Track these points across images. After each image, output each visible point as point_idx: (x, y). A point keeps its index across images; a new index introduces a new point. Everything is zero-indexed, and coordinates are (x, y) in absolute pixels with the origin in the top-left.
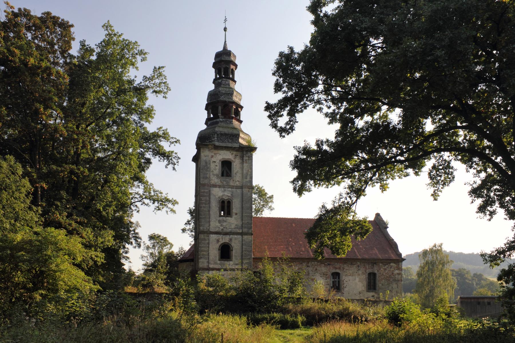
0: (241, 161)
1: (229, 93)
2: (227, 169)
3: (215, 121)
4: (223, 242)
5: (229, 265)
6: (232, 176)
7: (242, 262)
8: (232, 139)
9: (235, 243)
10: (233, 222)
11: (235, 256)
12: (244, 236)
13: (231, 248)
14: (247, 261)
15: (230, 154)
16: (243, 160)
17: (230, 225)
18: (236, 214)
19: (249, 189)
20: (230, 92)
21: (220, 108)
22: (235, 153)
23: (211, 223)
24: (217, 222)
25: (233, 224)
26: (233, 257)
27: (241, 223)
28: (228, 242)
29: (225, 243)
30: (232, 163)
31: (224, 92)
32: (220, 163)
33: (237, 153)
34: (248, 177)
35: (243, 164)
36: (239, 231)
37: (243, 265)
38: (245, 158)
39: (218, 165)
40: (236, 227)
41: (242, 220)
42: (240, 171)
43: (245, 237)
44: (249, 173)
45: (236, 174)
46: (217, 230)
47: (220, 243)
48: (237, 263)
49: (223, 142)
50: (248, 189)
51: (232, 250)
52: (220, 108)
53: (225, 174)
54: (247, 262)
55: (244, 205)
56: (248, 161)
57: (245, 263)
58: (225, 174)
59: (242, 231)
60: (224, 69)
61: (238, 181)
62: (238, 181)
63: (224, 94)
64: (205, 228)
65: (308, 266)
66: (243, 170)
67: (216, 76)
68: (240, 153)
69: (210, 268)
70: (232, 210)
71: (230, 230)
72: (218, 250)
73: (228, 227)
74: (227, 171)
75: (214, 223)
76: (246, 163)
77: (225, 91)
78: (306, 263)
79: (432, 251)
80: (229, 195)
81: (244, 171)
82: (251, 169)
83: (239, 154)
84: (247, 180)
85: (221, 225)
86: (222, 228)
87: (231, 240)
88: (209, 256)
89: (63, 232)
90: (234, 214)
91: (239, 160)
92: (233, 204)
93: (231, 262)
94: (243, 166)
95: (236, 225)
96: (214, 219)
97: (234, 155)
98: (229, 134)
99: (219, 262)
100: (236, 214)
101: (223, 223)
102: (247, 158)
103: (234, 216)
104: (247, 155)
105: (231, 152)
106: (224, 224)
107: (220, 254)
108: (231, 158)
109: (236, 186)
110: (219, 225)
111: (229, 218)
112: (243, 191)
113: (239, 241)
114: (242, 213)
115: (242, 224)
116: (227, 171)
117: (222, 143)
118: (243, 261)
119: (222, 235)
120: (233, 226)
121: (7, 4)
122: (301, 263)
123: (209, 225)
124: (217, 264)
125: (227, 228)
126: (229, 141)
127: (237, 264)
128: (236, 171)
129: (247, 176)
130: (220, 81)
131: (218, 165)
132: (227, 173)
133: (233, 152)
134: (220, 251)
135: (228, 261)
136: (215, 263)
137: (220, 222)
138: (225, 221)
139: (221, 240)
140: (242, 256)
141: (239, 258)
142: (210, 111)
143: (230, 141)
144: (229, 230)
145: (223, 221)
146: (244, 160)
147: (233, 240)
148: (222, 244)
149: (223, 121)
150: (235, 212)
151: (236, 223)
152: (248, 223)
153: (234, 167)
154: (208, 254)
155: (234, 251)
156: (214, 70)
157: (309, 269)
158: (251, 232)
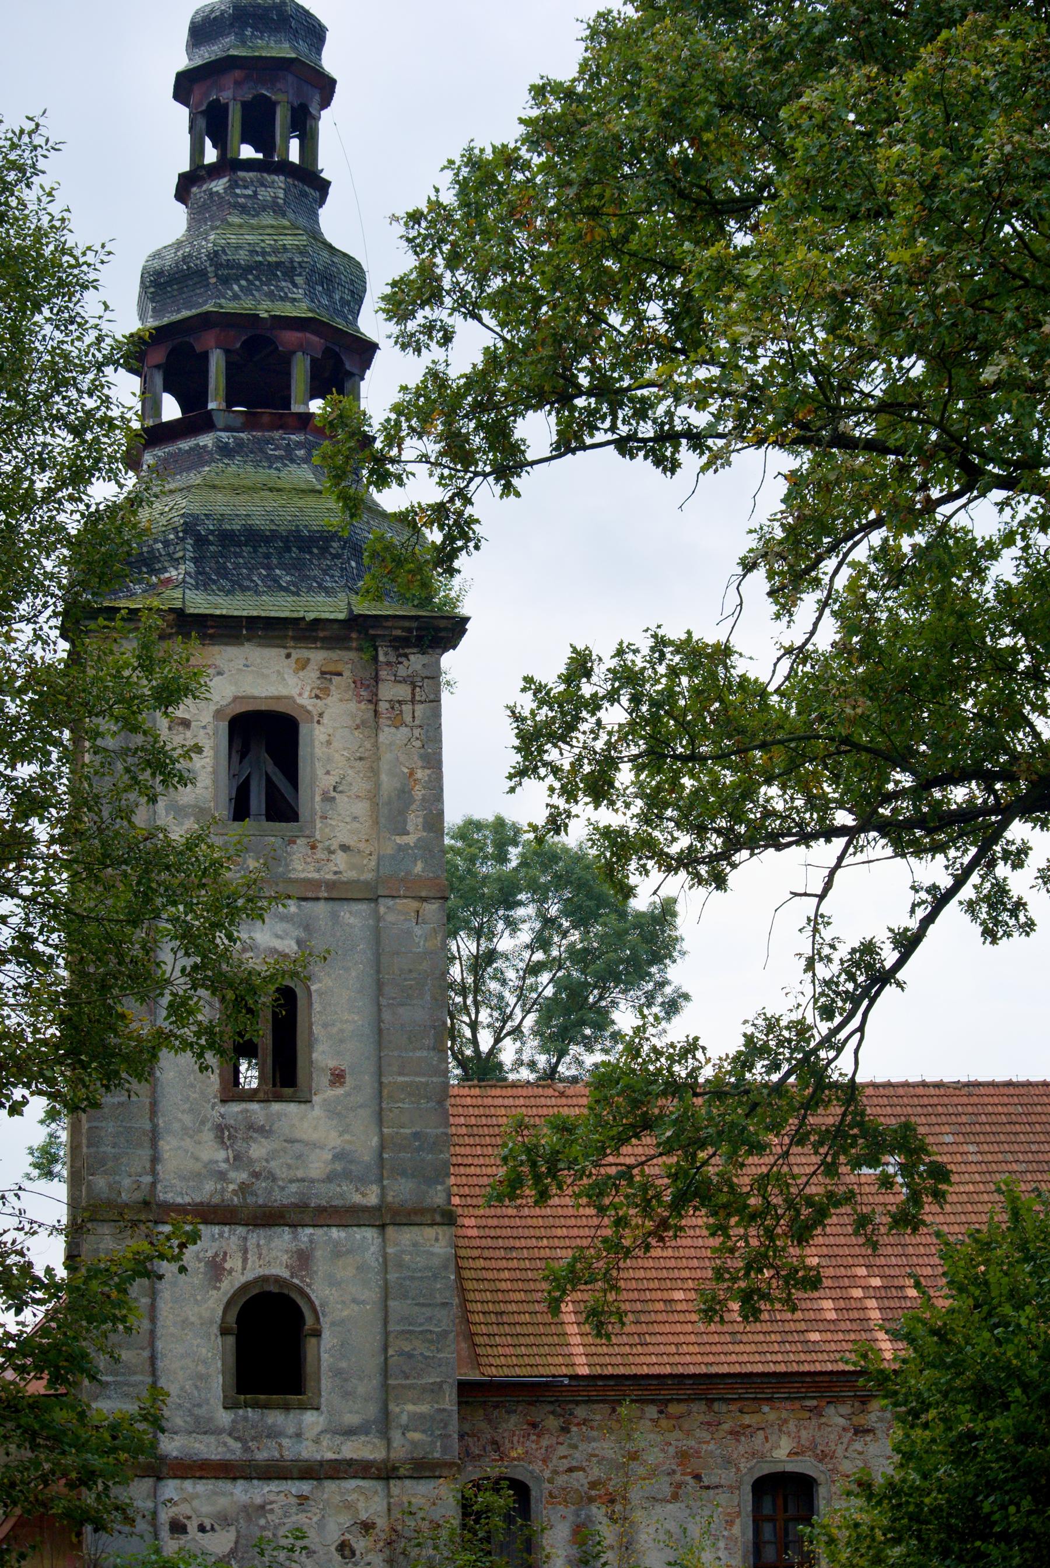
0: (358, 709)
1: (278, 264)
2: (271, 768)
3: (185, 445)
4: (249, 1276)
5: (299, 1435)
6: (303, 812)
7: (386, 1412)
8: (296, 567)
9: (333, 1282)
10: (315, 1136)
11: (338, 1373)
12: (390, 1230)
13: (309, 1321)
14: (424, 1408)
15: (287, 667)
16: (374, 700)
17: (299, 1157)
18: (338, 1078)
19: (424, 899)
20: (284, 257)
21: (217, 363)
22: (318, 657)
23: (167, 1146)
24: (208, 1136)
25: (314, 1145)
26: (326, 1384)
27: (375, 1141)
28: (285, 1274)
29: (264, 1279)
30: (303, 730)
31: (242, 256)
32: (224, 726)
33: (335, 655)
34: (414, 820)
35: (377, 728)
36: (357, 1199)
37: (396, 1435)
38: (389, 691)
39: (207, 744)
40: (338, 1167)
41: (380, 1121)
42: (359, 784)
43: (404, 1237)
44: (418, 793)
45: (327, 799)
46: (207, 1191)
47: (228, 1286)
48: (351, 1419)
49: (238, 586)
50: (415, 904)
51: (317, 1334)
52: (217, 363)
53: (257, 801)
54: (422, 1416)
55: (386, 1016)
56: (407, 708)
57: (404, 1419)
58: (257, 801)
59: (383, 1195)
60: (246, 106)
61: (345, 848)
62: (345, 848)
63: (248, 269)
64: (127, 1182)
65: (860, 1431)
66: (374, 772)
67: (197, 151)
68: (352, 655)
69: (162, 1459)
70: (310, 1047)
71: (294, 1188)
72: (215, 1330)
73: (282, 1173)
74: (269, 780)
75: (188, 1143)
76: (398, 722)
77: (253, 252)
78: (845, 1409)
79: (863, 59)
80: (289, 946)
81: (384, 777)
82: (434, 762)
83: (346, 660)
84: (410, 840)
85: (238, 1160)
86: (243, 1176)
87: (303, 1259)
88: (154, 1372)
89: (946, 882)
90: (321, 1081)
91: (352, 706)
92: (317, 1007)
93: (309, 1417)
94: (376, 745)
95: (339, 1156)
96: (187, 1119)
97: (312, 674)
98: (274, 535)
99: (225, 1418)
100: (338, 1078)
101: (247, 1139)
102: (403, 691)
103: (325, 1094)
104: (402, 671)
105: (296, 654)
106: (258, 1150)
107: (232, 1360)
108: (294, 692)
109: (331, 885)
110: (221, 1155)
111: (292, 1108)
112: (378, 918)
113: (361, 1268)
114: (380, 1073)
115: (382, 1147)
116: (269, 780)
117: (228, 593)
118: (393, 1407)
119: (241, 1230)
120: (317, 1166)
121: (751, 532)
122: (818, 1412)
123: (155, 1160)
124: (217, 1432)
125: (272, 1177)
126: (276, 580)
127: (350, 1432)
128: (332, 780)
129: (403, 812)
130: (219, 186)
131: (207, 744)
132: (271, 788)
133: (305, 654)
134: (231, 1340)
135: (287, 1408)
136: (203, 1427)
137: (223, 1133)
138: (264, 1131)
139: (233, 1263)
140: (385, 1372)
141: (367, 1386)
142: (159, 380)
143: (286, 579)
144: (285, 1195)
145: (251, 1127)
146: (383, 706)
147: (321, 1264)
148: (245, 1287)
149: (240, 443)
150: (332, 1064)
151: (334, 1140)
152: (416, 1135)
153: (319, 751)
154: (153, 1359)
155: (328, 1338)
156: (182, 113)
157: (873, 1449)
158: (439, 1200)
